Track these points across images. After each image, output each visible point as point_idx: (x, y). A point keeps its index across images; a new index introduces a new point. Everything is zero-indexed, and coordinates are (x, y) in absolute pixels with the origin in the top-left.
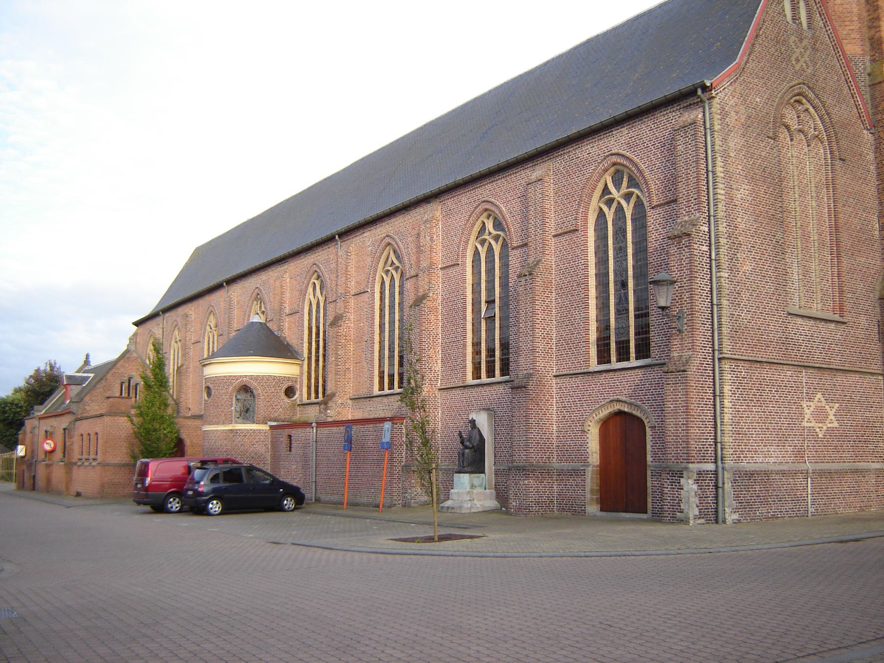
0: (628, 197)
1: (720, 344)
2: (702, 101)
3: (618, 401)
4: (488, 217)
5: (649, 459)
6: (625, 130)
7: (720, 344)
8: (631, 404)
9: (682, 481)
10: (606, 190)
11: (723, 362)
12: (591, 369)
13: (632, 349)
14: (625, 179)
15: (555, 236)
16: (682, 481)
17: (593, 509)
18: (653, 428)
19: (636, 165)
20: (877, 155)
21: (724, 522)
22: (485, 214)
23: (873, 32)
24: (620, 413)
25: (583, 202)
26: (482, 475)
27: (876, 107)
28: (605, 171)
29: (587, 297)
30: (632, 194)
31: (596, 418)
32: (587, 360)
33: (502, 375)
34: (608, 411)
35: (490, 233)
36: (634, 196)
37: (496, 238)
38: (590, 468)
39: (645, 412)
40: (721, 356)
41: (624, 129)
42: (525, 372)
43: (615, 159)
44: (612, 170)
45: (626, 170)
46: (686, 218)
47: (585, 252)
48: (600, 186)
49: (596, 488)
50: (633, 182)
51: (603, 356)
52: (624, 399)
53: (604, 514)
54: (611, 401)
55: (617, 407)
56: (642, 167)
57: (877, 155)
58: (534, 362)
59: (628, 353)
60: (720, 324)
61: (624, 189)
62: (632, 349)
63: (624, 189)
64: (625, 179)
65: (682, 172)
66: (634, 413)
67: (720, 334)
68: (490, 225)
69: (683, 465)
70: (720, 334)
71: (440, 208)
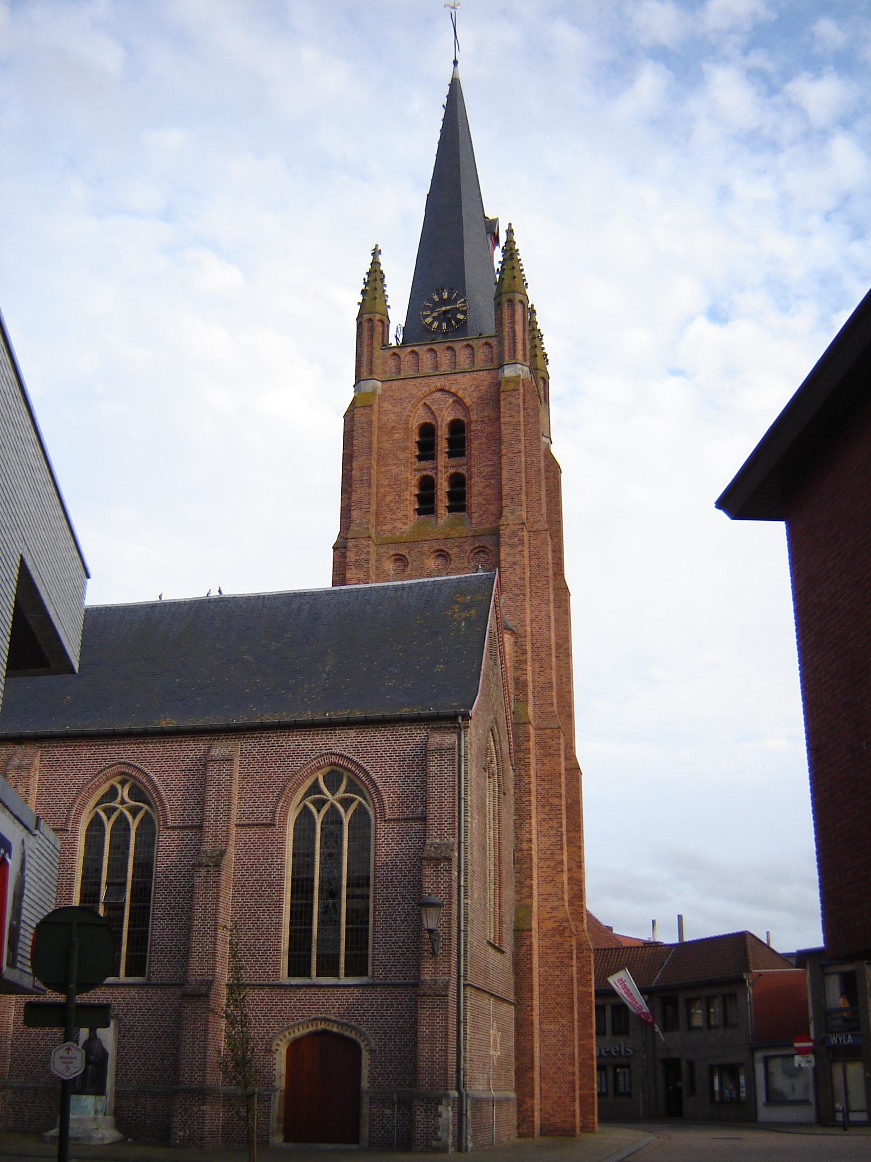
0: (346, 802)
1: (465, 971)
2: (459, 728)
3: (325, 1020)
4: (123, 783)
5: (365, 1084)
6: (352, 733)
7: (465, 971)
8: (343, 1024)
9: (440, 1108)
10: (315, 788)
11: (468, 988)
12: (281, 981)
13: (342, 965)
14: (344, 783)
15: (237, 825)
16: (440, 1108)
17: (278, 1139)
18: (371, 1051)
19: (366, 773)
20: (517, 791)
21: (466, 1150)
22: (119, 778)
23: (520, 672)
24: (324, 1032)
25: (283, 793)
26: (104, 1097)
27: (519, 746)
28: (319, 768)
29: (280, 900)
30: (352, 800)
31: (288, 1037)
32: (277, 972)
33: (127, 974)
34: (307, 1030)
35: (123, 802)
36: (356, 803)
37: (134, 811)
38: (278, 1094)
39: (362, 1034)
40: (467, 982)
41: (352, 731)
42: (199, 978)
43: (334, 759)
44: (328, 769)
45: (345, 774)
46: (438, 841)
47: (281, 850)
48: (308, 783)
49: (282, 1116)
50: (352, 787)
51: (298, 966)
52: (333, 1018)
53: (285, 1145)
54: (315, 1019)
55: (321, 1026)
56: (374, 776)
57: (517, 791)
58: (214, 967)
59: (338, 968)
60: (465, 951)
61: (340, 794)
62: (342, 965)
63: (340, 794)
64: (344, 783)
65: (434, 792)
66: (347, 1034)
67: (465, 960)
68: (124, 792)
69: (442, 1092)
70: (465, 960)
71: (39, 754)
